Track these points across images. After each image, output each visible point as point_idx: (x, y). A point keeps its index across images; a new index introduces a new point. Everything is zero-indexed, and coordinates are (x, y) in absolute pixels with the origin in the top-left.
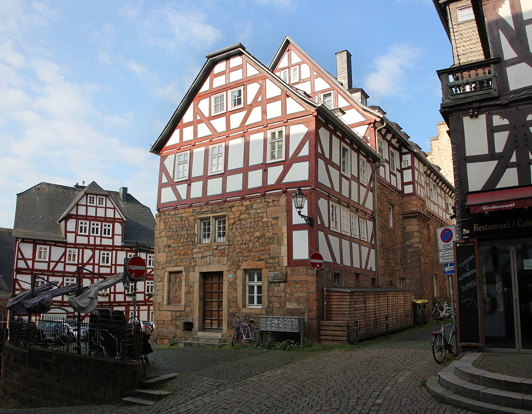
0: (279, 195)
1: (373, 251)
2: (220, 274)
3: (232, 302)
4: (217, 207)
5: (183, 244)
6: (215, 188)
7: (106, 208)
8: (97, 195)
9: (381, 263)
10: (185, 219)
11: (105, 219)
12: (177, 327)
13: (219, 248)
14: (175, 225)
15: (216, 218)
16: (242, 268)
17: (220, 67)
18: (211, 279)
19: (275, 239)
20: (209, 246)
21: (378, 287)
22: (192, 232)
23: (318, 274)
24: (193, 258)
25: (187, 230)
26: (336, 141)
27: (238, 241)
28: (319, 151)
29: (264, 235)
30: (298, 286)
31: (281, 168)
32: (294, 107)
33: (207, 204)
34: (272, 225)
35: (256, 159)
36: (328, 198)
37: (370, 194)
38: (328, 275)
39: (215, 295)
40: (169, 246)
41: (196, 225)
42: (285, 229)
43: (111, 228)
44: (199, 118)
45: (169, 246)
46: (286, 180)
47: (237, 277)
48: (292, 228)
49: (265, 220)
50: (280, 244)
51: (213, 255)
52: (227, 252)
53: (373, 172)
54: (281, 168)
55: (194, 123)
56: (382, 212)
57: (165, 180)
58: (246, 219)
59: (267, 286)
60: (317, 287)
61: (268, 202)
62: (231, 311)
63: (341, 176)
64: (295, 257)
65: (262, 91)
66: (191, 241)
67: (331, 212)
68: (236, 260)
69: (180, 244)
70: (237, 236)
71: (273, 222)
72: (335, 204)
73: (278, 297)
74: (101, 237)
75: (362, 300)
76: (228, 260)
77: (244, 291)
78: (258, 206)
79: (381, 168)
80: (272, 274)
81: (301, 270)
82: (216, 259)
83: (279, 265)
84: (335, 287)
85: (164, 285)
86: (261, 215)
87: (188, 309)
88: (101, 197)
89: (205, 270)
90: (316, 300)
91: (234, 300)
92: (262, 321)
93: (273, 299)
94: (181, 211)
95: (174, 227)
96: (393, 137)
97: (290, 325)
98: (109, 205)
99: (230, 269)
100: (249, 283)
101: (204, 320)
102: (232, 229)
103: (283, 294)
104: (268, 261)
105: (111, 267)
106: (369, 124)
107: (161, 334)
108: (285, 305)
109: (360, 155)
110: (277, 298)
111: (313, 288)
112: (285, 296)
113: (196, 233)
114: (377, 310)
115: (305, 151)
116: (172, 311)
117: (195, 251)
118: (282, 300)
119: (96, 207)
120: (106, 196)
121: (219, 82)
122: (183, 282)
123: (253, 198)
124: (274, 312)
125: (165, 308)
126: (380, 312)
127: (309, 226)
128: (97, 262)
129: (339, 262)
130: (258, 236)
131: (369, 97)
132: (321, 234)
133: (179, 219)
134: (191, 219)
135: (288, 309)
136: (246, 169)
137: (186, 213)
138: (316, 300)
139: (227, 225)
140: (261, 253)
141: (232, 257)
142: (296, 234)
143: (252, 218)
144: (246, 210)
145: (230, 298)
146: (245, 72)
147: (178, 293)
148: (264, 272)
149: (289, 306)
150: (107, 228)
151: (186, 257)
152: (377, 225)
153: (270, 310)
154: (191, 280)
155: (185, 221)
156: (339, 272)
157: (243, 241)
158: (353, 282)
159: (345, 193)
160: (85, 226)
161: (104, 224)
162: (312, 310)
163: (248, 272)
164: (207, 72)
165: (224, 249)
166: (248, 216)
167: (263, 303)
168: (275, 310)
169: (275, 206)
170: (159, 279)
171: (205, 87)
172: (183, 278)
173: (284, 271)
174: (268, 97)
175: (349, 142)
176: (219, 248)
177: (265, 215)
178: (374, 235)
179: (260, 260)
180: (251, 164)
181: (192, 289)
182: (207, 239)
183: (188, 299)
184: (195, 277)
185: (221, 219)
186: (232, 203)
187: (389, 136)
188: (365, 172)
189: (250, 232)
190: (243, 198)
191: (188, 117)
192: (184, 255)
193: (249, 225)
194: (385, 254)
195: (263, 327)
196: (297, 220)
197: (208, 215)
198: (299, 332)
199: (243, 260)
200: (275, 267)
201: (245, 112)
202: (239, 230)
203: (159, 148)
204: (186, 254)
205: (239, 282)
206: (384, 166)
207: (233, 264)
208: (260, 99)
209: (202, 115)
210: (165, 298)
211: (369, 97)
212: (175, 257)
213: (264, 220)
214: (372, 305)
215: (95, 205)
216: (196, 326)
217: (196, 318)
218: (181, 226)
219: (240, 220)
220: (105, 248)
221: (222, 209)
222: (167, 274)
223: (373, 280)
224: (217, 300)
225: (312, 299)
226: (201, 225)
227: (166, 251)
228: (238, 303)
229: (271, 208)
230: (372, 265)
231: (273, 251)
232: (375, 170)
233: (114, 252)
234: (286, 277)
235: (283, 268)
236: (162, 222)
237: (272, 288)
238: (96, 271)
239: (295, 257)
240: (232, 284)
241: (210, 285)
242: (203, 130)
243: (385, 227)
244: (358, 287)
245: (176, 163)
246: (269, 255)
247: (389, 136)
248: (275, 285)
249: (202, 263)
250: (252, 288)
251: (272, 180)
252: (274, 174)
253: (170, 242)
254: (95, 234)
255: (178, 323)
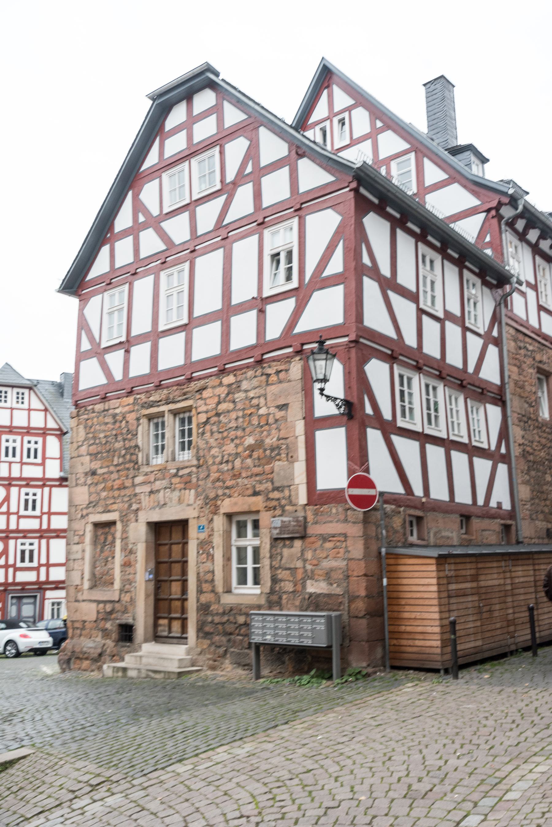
0: (288, 358)
1: (502, 468)
2: (183, 524)
3: (206, 581)
4: (175, 393)
5: (118, 468)
6: (172, 354)
7: (29, 410)
8: (13, 387)
9: (524, 492)
10: (121, 418)
11: (28, 431)
12: (106, 633)
13: (181, 473)
14: (104, 431)
15: (175, 413)
16: (222, 511)
17: (177, 116)
18: (167, 534)
19: (281, 450)
20: (163, 470)
21: (518, 543)
22: (133, 444)
23: (366, 520)
24: (135, 495)
25: (124, 440)
26: (405, 243)
27: (214, 457)
28: (366, 260)
29: (262, 441)
30: (328, 545)
31: (290, 304)
32: (312, 176)
33: (159, 387)
34: (276, 421)
35: (243, 291)
36: (391, 359)
37: (493, 351)
38: (392, 522)
39: (177, 568)
40: (94, 473)
41: (140, 428)
42: (300, 427)
43: (39, 446)
44: (141, 219)
45: (94, 473)
46: (301, 327)
47: (212, 530)
48: (314, 424)
49: (263, 411)
50: (291, 459)
51: (170, 487)
52: (194, 480)
53: (498, 305)
54: (290, 304)
55: (134, 231)
56: (522, 387)
57: (86, 346)
58: (228, 412)
59: (268, 546)
60: (367, 547)
61: (268, 375)
62: (204, 599)
63: (421, 312)
64: (322, 484)
65: (252, 153)
66: (130, 461)
67: (397, 388)
68: (212, 495)
69: (112, 468)
70: (211, 448)
71: (279, 414)
72: (407, 373)
73: (289, 569)
74: (22, 463)
75: (469, 572)
76: (197, 495)
77: (227, 559)
78: (250, 383)
79: (516, 297)
80: (277, 522)
81: (334, 511)
82: (177, 493)
83: (291, 503)
84: (412, 545)
85: (83, 551)
86: (255, 402)
87: (126, 598)
88: (21, 391)
89: (156, 517)
90: (365, 575)
91: (209, 577)
92: (257, 623)
93: (282, 574)
94: (114, 403)
95: (102, 435)
96: (542, 237)
97: (311, 631)
98: (36, 404)
99: (202, 514)
100: (236, 542)
101: (157, 618)
102: (203, 433)
103: (299, 564)
104: (271, 495)
105: (40, 517)
106: (488, 211)
107: (77, 650)
108: (304, 587)
109: (465, 272)
110: (288, 572)
111: (357, 549)
112: (304, 567)
113: (140, 444)
114: (509, 593)
115: (336, 265)
116: (99, 602)
117: (138, 480)
118: (300, 574)
119: (12, 409)
120: (30, 388)
121: (175, 145)
122: (118, 543)
123: (241, 369)
124: (284, 601)
125: (86, 595)
126: (516, 598)
127: (345, 418)
128: (13, 509)
129: (418, 491)
130: (250, 446)
131: (488, 160)
132: (374, 436)
133: (109, 420)
134: (131, 417)
135: (311, 595)
136: (226, 313)
137: (121, 406)
138: (365, 575)
139: (194, 426)
140: (258, 478)
141: (204, 491)
142: (322, 437)
143: (239, 410)
144: (228, 394)
145: (202, 574)
146: (220, 121)
147: (109, 566)
148: (265, 518)
149: (312, 588)
150: (33, 446)
151: (122, 494)
152: (509, 413)
153: (275, 598)
154: (132, 539)
155: (121, 422)
156: (419, 513)
157: (223, 457)
158: (454, 535)
159: (431, 348)
160: (36, 446)
161: (26, 439)
162: (358, 596)
163: (235, 519)
164: (153, 129)
165: (190, 474)
166: (231, 406)
167: (262, 582)
168: (284, 597)
169: (280, 382)
170: (76, 539)
171: (152, 159)
172: (118, 535)
173: (301, 514)
174: (263, 164)
175: (438, 244)
176: (181, 473)
177: (262, 400)
178: (504, 434)
179: (256, 494)
180: (235, 301)
181: (132, 557)
182: (160, 455)
183: (127, 577)
184: (139, 532)
185: (183, 415)
186: (202, 382)
187: (533, 235)
188: (479, 305)
189: (236, 438)
190: (223, 371)
191: (123, 220)
192: (119, 489)
193: (233, 424)
194: (533, 473)
195: (258, 635)
196: (323, 408)
197: (162, 409)
198: (330, 647)
199: (224, 494)
200: (283, 507)
201: (224, 197)
202: (216, 436)
203: (76, 283)
204: (123, 487)
205: (218, 540)
206: (523, 294)
207: (207, 504)
208: (249, 169)
209: (146, 212)
210: (87, 576)
211: (488, 160)
212: (104, 494)
213: (261, 412)
214: (496, 582)
215: (8, 405)
216: (140, 631)
217: (141, 616)
218: (114, 432)
219: (218, 415)
220: (28, 482)
221: (185, 394)
222: (89, 528)
223: (507, 528)
224: (178, 578)
225: (355, 574)
226: (149, 430)
227: (89, 482)
228: (216, 583)
229: (273, 387)
230: (501, 496)
231: (278, 474)
232: (503, 302)
233: (46, 490)
234: (305, 528)
235: (299, 508)
236: (81, 427)
237: (279, 551)
238: (13, 526)
239: (322, 484)
240: (205, 545)
241: (167, 547)
242: (151, 243)
243: (530, 418)
244: (468, 543)
245: (105, 311)
246: (273, 483)
247: (533, 235)
248: (284, 546)
249: (152, 504)
250: (241, 551)
251: (274, 331)
252: (278, 316)
253: (96, 465)
254: (10, 458)
255: (108, 625)
